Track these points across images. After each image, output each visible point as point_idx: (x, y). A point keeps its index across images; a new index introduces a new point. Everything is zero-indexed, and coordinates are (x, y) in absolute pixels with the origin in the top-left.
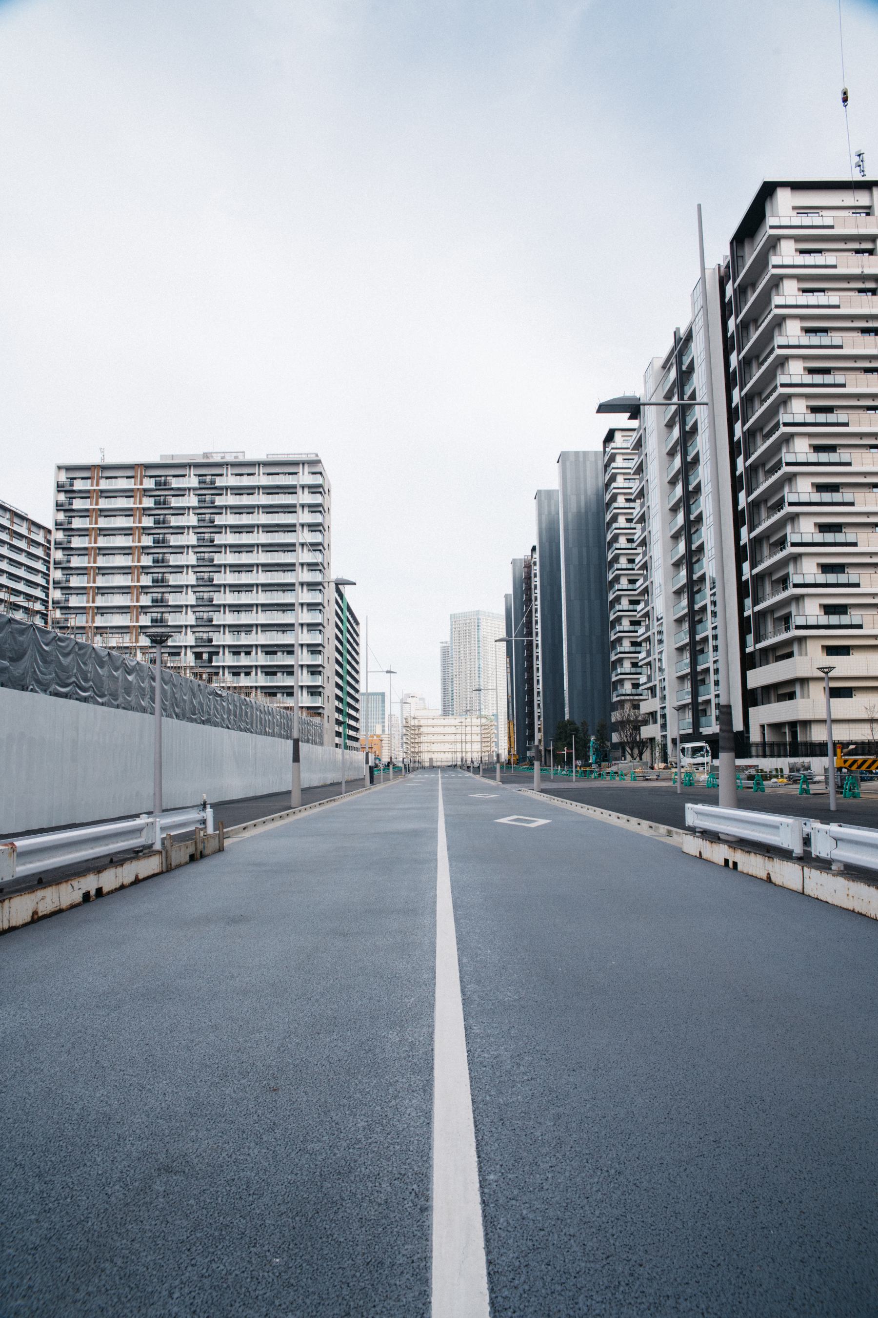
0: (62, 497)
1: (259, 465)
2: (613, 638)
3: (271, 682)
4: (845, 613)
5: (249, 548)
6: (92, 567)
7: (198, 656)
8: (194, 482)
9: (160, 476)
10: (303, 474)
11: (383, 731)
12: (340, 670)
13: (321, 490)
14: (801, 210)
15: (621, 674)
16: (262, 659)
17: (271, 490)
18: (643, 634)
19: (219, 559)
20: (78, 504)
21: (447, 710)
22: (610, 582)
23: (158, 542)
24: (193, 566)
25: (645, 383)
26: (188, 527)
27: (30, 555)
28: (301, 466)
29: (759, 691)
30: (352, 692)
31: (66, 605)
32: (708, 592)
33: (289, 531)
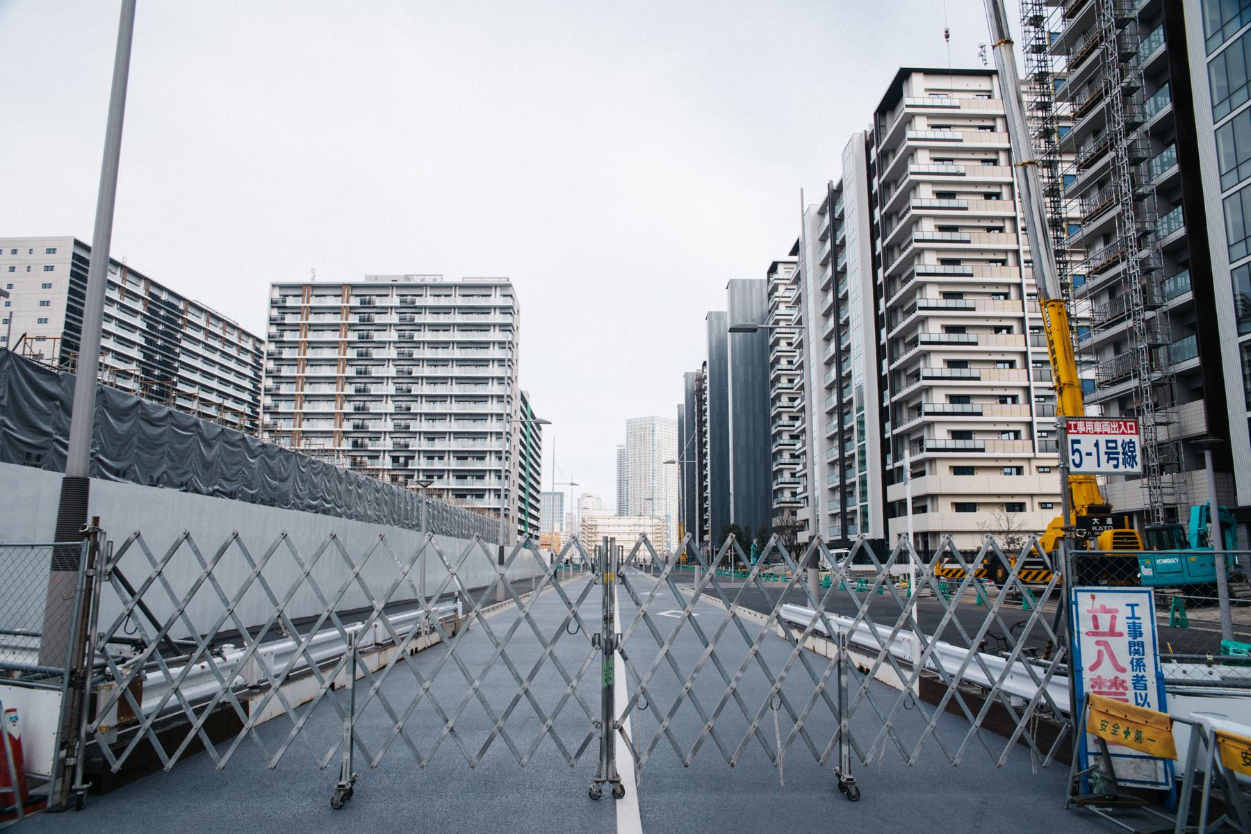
0: (275, 313)
1: (456, 287)
2: (774, 450)
3: (461, 485)
4: (970, 438)
5: (446, 327)
6: (300, 377)
7: (395, 459)
8: (396, 301)
9: (365, 295)
10: (495, 296)
11: (561, 529)
12: (523, 473)
13: (511, 311)
14: (933, 92)
15: (781, 483)
16: (454, 464)
17: (465, 310)
18: (801, 448)
19: (417, 372)
20: (289, 319)
21: (622, 511)
22: (772, 399)
23: (363, 338)
24: (393, 378)
25: (844, 162)
26: (390, 342)
27: (240, 361)
28: (493, 289)
29: (897, 505)
30: (534, 493)
31: (275, 411)
32: (855, 415)
33: (481, 331)
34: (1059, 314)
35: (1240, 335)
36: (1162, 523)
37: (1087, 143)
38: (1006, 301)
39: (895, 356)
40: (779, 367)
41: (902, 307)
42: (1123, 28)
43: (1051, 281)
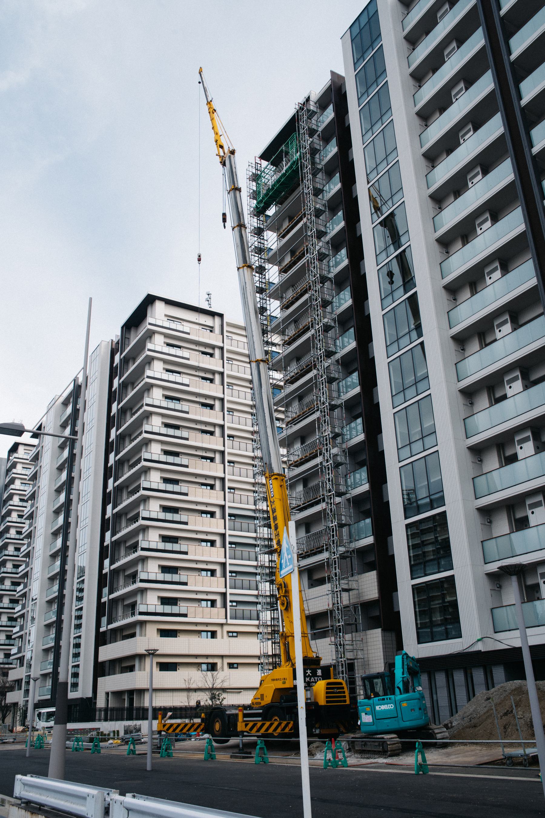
29: (107, 665)
34: (281, 486)
35: (406, 518)
36: (159, 712)
37: (291, 365)
38: (212, 491)
39: (117, 529)
40: (8, 536)
41: (127, 487)
42: (323, 284)
43: (275, 457)
